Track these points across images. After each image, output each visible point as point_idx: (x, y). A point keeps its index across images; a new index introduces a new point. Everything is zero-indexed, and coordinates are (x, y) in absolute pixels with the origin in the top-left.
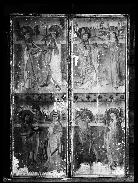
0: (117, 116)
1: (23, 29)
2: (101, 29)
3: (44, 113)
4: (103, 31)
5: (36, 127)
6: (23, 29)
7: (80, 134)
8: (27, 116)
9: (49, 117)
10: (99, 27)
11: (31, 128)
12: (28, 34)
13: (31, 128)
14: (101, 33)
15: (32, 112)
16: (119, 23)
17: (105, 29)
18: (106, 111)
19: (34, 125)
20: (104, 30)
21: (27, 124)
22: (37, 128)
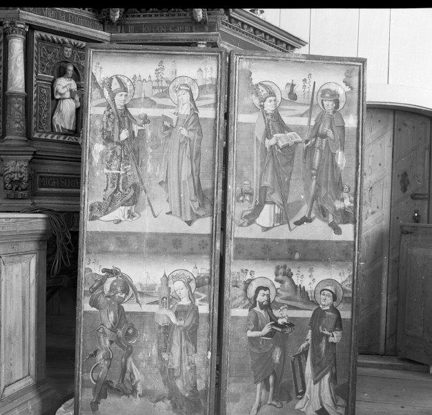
0: (190, 288)
1: (260, 87)
2: (158, 81)
3: (302, 287)
4: (162, 88)
5: (282, 318)
6: (260, 87)
7: (101, 331)
8: (262, 292)
9: (313, 295)
10: (154, 78)
11: (271, 320)
12: (271, 101)
13: (271, 320)
14: (156, 91)
15: (274, 282)
16: (200, 70)
17: (167, 82)
18: (165, 275)
19: (276, 313)
20: (164, 84)
21: (262, 309)
22: (285, 321)
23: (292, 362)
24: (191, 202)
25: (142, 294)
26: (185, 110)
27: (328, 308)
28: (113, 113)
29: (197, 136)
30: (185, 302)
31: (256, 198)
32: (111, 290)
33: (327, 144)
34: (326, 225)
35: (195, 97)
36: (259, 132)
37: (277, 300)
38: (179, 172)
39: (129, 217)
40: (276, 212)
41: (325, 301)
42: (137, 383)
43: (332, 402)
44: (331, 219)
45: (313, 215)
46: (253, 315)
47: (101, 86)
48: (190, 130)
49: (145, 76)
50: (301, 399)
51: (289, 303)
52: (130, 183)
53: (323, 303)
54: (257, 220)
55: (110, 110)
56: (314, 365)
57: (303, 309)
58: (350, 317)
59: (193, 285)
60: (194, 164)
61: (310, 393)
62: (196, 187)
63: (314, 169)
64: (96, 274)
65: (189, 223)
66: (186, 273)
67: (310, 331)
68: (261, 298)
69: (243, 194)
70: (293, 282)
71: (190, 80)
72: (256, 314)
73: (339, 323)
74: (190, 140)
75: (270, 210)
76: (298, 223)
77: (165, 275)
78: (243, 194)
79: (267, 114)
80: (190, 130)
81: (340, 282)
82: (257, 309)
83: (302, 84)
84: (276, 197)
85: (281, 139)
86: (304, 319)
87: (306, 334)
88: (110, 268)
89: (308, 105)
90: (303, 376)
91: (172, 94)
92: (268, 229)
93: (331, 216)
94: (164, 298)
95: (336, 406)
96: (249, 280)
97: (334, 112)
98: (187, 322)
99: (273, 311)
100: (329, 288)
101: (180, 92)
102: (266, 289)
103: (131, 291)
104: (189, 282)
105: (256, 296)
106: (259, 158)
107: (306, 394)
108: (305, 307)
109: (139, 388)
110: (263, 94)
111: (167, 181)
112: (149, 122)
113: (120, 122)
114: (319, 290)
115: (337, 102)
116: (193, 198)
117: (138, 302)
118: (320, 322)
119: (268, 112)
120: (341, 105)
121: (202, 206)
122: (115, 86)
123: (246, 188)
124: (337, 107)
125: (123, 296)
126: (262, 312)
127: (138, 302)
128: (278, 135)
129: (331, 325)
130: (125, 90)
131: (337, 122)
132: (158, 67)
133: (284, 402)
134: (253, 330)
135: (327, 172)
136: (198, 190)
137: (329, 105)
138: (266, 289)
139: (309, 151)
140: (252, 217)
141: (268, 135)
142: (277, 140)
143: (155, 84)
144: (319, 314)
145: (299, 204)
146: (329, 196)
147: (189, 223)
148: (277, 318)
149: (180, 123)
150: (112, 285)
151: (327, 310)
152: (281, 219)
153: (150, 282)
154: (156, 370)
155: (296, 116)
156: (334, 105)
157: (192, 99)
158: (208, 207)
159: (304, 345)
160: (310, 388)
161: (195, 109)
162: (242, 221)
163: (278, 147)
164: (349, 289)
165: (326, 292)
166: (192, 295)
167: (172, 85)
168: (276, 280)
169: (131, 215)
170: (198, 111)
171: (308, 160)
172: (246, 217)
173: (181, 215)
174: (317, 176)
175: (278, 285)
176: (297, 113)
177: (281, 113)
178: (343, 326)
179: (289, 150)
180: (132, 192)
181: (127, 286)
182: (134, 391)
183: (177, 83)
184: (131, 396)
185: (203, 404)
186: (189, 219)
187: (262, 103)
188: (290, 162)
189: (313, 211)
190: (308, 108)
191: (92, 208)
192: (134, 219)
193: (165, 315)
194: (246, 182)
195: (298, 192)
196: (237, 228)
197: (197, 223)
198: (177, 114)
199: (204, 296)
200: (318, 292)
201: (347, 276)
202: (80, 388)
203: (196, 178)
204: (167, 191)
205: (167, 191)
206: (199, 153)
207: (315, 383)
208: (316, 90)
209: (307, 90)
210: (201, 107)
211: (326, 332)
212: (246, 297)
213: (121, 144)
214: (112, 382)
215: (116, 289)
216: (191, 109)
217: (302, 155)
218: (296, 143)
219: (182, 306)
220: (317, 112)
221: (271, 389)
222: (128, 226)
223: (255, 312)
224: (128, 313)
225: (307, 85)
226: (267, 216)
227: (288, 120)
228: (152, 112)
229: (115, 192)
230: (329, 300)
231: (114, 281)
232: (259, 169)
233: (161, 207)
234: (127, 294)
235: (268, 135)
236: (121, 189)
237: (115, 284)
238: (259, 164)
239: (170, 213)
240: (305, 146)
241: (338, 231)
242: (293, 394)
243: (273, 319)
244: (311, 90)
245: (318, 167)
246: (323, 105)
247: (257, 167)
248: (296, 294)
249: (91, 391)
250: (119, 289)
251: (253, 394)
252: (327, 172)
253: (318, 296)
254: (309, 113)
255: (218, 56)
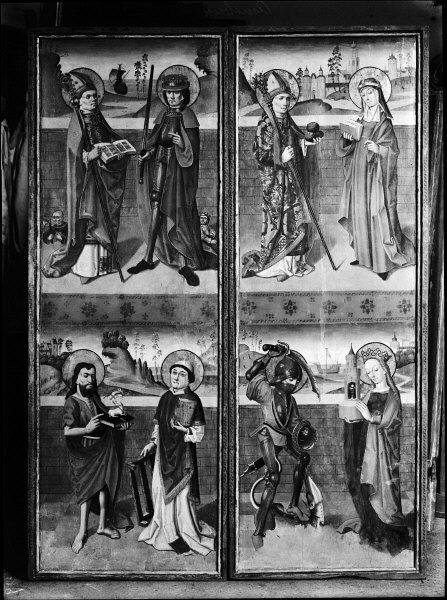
1: (73, 77)
2: (332, 75)
3: (143, 362)
4: (339, 85)
5: (115, 407)
6: (73, 77)
8: (84, 371)
9: (159, 373)
10: (327, 71)
11: (99, 412)
12: (89, 96)
14: (331, 90)
16: (393, 57)
17: (345, 76)
18: (352, 352)
19: (106, 401)
20: (342, 80)
22: (119, 411)
23: (132, 472)
24: (385, 246)
25: (320, 378)
26: (373, 116)
27: (182, 392)
28: (270, 124)
29: (391, 152)
30: (382, 388)
31: (71, 236)
32: (277, 374)
33: (173, 154)
34: (175, 272)
35: (386, 97)
36: (73, 143)
37: (107, 381)
38: (368, 204)
39: (298, 271)
40: (102, 255)
41: (178, 383)
42: (316, 505)
43: (193, 530)
44: (182, 264)
45: (155, 259)
46: (72, 405)
47: (252, 86)
48: (382, 144)
49: (313, 69)
50: (147, 525)
51: (123, 386)
52: (298, 224)
53: (175, 385)
54: (74, 268)
55: (267, 120)
56: (164, 477)
57: (145, 395)
58: (215, 405)
59: (392, 364)
60: (388, 192)
61: (160, 517)
62: (392, 224)
63: (155, 192)
64: (255, 353)
65: (384, 276)
66: (383, 348)
67: (157, 427)
68: (83, 380)
69: (53, 230)
70: (128, 354)
71: (378, 72)
72: (77, 403)
73: (199, 414)
74: (381, 158)
75: (93, 252)
76: (133, 271)
77: (352, 352)
78: (53, 230)
79: (84, 116)
80: (382, 144)
81: (198, 353)
82: (78, 396)
83: (133, 69)
84: (100, 234)
85: (103, 151)
86: (147, 409)
87: (150, 431)
88: (274, 343)
89: (144, 99)
90: (148, 492)
91: (353, 92)
92: (90, 280)
93: (182, 259)
94: (352, 383)
95: (200, 536)
96: (65, 354)
97: (182, 109)
98: (388, 415)
99: (102, 398)
100: (183, 363)
101: (365, 91)
102: (89, 366)
103: (305, 376)
104: (386, 361)
105: (75, 377)
106: (74, 178)
107: (155, 518)
108: (148, 391)
109: (320, 514)
110: (77, 87)
111: (350, 215)
112: (321, 135)
113: (280, 136)
114: (168, 366)
115: (186, 94)
116: (388, 240)
117: (314, 390)
118: (171, 413)
119: (86, 112)
120: (193, 97)
121: (402, 250)
122: (273, 84)
123: (55, 222)
124: (187, 100)
125: (294, 382)
126: (86, 400)
127: (314, 390)
128: (101, 145)
129: (187, 418)
130: (287, 90)
131: (187, 123)
132: (332, 57)
133: (122, 531)
134: (72, 427)
135: (174, 194)
136: (398, 233)
137: (174, 98)
138: (89, 366)
139: (147, 166)
140: (66, 265)
141: (86, 145)
142: (100, 150)
143: (329, 80)
144: (169, 403)
145: (133, 244)
146: (178, 230)
147: (384, 276)
148: (108, 408)
149: (366, 134)
150: (278, 366)
151: (181, 396)
152: (109, 264)
153: (331, 362)
154: (344, 487)
155: (127, 116)
156: (183, 98)
157: (382, 99)
158: (411, 252)
159: (148, 447)
160: (160, 509)
161: (386, 114)
162: (51, 270)
163: (102, 162)
164: (214, 364)
165: (179, 370)
166: (392, 378)
167: (353, 81)
168: (105, 354)
169: (301, 268)
170: (390, 115)
171: (146, 178)
172: (58, 264)
173: (372, 265)
174: (159, 201)
175: (107, 361)
176: (128, 111)
177: (103, 112)
178: (206, 417)
179: (119, 165)
180: (302, 235)
181: (298, 367)
182: (313, 517)
183: (356, 80)
184: (309, 526)
185: (411, 534)
186: (383, 271)
187: (76, 100)
188: (120, 183)
189: (156, 252)
190: (145, 103)
191: (245, 262)
192: (306, 273)
193: (353, 409)
194: (56, 214)
195: (137, 220)
196: (46, 280)
197: (393, 277)
198: (361, 121)
199: (408, 379)
200: (166, 369)
201: (209, 344)
202: (237, 515)
203: (391, 212)
204: (351, 232)
205: (351, 232)
206: (394, 176)
207: (167, 502)
208: (155, 77)
209: (141, 78)
210: (395, 109)
211: (181, 428)
212: (61, 379)
213: (284, 168)
214: (281, 506)
215: (283, 373)
216: (381, 114)
217: (137, 171)
218: (128, 155)
219: (377, 395)
220: (157, 111)
221: (102, 511)
222: (296, 284)
223: (74, 401)
224: (301, 406)
225: (142, 71)
226: (87, 260)
227: (115, 123)
228: (324, 120)
229: (278, 236)
230: (184, 381)
231: (280, 362)
232: (75, 194)
233: (343, 253)
234: (300, 380)
235: (86, 145)
236: (285, 232)
237: (282, 366)
238: (75, 187)
239: (355, 263)
240: (141, 158)
241: (193, 281)
242: (135, 519)
243: (103, 410)
244: (148, 77)
245: (161, 188)
246: (166, 98)
247: (71, 191)
248: (134, 373)
249: (252, 519)
250: (287, 372)
251: (75, 518)
252: (174, 194)
253: (166, 375)
254: (145, 113)
255: (417, 36)
